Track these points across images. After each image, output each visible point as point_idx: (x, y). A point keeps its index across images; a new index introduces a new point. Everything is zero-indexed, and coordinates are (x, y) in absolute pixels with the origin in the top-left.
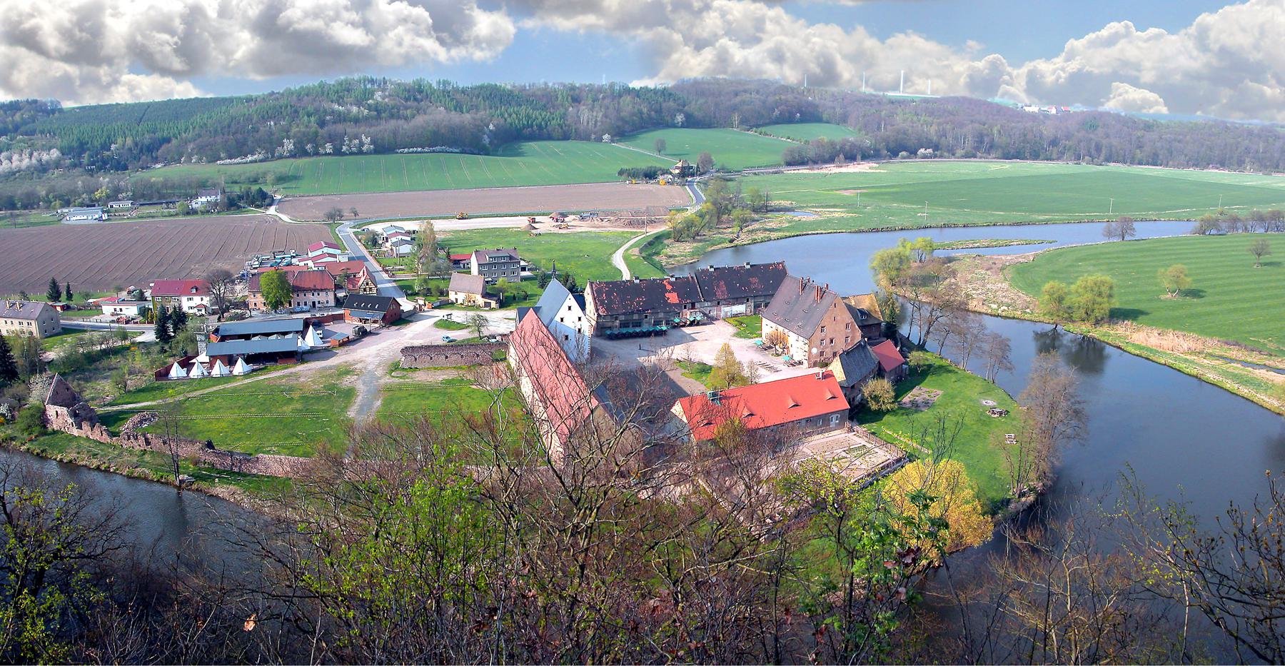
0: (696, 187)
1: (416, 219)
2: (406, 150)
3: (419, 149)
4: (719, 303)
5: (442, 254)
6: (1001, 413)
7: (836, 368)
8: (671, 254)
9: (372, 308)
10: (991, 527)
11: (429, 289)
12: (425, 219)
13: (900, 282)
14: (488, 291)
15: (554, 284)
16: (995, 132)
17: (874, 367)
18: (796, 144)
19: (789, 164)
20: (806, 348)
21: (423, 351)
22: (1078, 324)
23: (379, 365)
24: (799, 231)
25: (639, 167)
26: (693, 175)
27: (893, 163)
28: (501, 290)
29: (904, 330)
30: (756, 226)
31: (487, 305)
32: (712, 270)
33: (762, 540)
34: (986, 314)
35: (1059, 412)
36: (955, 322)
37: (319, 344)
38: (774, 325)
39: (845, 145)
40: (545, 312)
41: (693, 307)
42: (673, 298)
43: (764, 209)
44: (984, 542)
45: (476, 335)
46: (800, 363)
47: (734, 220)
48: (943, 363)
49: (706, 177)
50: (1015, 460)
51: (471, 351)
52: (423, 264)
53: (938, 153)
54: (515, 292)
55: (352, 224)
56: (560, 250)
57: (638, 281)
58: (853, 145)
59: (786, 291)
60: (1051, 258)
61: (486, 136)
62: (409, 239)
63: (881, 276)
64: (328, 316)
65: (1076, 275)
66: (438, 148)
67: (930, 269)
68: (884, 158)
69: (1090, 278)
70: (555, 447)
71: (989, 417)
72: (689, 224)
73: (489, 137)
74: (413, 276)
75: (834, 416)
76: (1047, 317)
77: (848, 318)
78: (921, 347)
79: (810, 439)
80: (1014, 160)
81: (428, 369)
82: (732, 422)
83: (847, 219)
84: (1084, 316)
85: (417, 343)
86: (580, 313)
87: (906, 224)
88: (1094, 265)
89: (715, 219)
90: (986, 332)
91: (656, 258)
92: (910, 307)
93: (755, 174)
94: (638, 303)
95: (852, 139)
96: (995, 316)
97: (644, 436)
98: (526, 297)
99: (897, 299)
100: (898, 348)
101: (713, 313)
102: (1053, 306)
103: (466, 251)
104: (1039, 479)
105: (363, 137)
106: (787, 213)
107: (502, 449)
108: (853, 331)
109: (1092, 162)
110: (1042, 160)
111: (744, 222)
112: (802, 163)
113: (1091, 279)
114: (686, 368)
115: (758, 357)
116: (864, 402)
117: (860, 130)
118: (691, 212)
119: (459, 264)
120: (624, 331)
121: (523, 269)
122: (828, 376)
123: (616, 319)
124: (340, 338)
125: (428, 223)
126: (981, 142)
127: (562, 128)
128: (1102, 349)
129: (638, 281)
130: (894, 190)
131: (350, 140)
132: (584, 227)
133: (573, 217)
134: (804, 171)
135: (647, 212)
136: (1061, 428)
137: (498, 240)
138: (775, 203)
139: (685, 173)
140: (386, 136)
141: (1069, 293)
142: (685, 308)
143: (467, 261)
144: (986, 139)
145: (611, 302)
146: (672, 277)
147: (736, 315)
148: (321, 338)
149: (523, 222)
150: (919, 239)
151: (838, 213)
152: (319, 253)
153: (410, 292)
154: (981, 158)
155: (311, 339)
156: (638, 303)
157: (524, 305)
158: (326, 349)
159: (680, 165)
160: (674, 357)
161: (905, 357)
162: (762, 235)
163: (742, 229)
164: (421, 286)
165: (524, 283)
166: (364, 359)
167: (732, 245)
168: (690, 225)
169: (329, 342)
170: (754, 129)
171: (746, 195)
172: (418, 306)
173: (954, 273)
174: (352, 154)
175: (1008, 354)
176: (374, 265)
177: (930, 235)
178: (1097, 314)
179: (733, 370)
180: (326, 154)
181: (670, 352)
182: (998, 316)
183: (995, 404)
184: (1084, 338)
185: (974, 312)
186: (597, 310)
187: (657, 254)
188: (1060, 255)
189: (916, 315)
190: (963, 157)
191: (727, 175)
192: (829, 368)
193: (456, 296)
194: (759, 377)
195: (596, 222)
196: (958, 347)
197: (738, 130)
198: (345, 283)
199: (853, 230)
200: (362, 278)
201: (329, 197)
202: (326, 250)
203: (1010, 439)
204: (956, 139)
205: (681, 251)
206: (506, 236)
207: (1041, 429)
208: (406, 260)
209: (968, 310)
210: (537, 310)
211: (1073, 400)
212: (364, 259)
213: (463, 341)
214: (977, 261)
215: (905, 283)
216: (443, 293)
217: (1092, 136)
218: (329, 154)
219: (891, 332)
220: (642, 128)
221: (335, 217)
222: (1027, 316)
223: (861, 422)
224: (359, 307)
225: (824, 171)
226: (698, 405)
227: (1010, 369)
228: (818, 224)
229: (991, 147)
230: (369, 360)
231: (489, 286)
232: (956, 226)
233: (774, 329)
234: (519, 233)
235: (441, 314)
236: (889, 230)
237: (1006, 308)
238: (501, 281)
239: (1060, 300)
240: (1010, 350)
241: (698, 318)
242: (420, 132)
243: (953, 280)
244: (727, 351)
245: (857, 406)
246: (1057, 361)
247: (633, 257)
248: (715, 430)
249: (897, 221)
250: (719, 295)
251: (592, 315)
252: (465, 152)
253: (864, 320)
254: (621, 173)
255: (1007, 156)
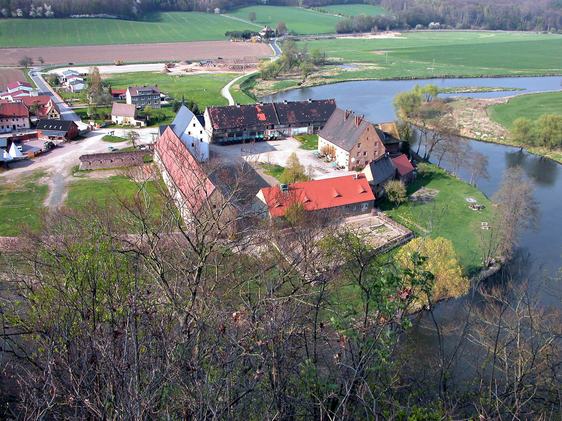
0: (275, 44)
1: (87, 66)
2: (77, 16)
3: (87, 16)
4: (290, 126)
5: (106, 90)
6: (479, 208)
7: (367, 172)
8: (260, 88)
9: (57, 129)
10: (468, 285)
11: (97, 115)
12: (93, 65)
13: (413, 115)
14: (138, 115)
15: (184, 109)
16: (485, 10)
17: (393, 172)
18: (345, 18)
19: (340, 32)
20: (348, 157)
21: (95, 158)
22: (537, 148)
23: (64, 169)
24: (344, 79)
25: (238, 30)
26: (274, 36)
27: (412, 32)
28: (147, 114)
29: (414, 148)
30: (316, 74)
31: (138, 124)
32: (286, 103)
33: (312, 284)
34: (473, 139)
35: (520, 209)
36: (450, 144)
37: (20, 155)
38: (327, 142)
39: (379, 19)
40: (178, 128)
41: (273, 128)
42: (262, 117)
43: (322, 63)
44: (462, 295)
45: (132, 145)
46: (343, 168)
47: (301, 70)
48: (441, 171)
49: (282, 38)
50: (487, 241)
51: (129, 157)
52: (92, 97)
53: (443, 25)
54: (157, 116)
55: (40, 68)
56: (187, 86)
57: (239, 106)
58: (384, 19)
59: (335, 119)
60: (521, 101)
61: (134, 8)
62: (82, 79)
63: (400, 111)
64: (25, 135)
65: (538, 113)
66: (101, 15)
67: (435, 106)
68: (406, 28)
69: (549, 115)
70: (185, 214)
71: (471, 210)
72: (272, 69)
73: (137, 8)
74: (86, 106)
75: (365, 204)
76: (516, 142)
77: (376, 138)
78: (426, 160)
79: (347, 219)
80: (498, 31)
81: (100, 170)
82: (297, 206)
83: (378, 71)
84: (543, 142)
85: (91, 152)
86: (201, 128)
87: (419, 75)
88: (552, 107)
89: (288, 66)
90: (471, 151)
91: (251, 91)
92: (419, 132)
93: (316, 39)
94: (240, 121)
95: (383, 15)
96: (478, 140)
97: (238, 211)
98: (165, 119)
99: (410, 126)
100: (410, 161)
101: (286, 132)
102: (520, 135)
103: (122, 88)
104: (503, 254)
105: (46, 6)
106: (338, 66)
107: (148, 221)
108: (380, 146)
109: (556, 31)
110: (519, 30)
111: (308, 72)
112: (348, 31)
113: (550, 116)
114: (266, 168)
115: (315, 163)
116: (385, 196)
117: (389, 9)
118: (273, 60)
119: (118, 97)
120: (231, 139)
121: (163, 99)
122: (361, 177)
123: (226, 131)
124: (36, 151)
125: (95, 68)
126: (475, 17)
127: (187, 3)
128: (555, 166)
129: (239, 106)
130: (410, 51)
131: (36, 7)
132: (203, 71)
133: (196, 64)
134: (350, 37)
135: (245, 60)
136: (521, 220)
137: (145, 80)
138: (329, 59)
139: (269, 35)
140: (62, 4)
141: (533, 126)
142: (267, 128)
143: (123, 95)
144: (478, 16)
145: (222, 120)
146: (261, 103)
147: (301, 134)
148: (21, 151)
149: (161, 67)
150: (427, 85)
151: (372, 67)
152: (16, 90)
153: (84, 117)
154: (474, 29)
155: (14, 152)
156: (240, 121)
157: (164, 124)
158: (26, 159)
159: (265, 29)
160: (259, 160)
161: (415, 166)
162: (321, 81)
163: (306, 76)
164: (91, 112)
165: (163, 109)
166: (53, 165)
167: (300, 87)
168: (272, 69)
169: (27, 154)
170: (312, 8)
171: (310, 53)
172: (90, 127)
173: (451, 110)
174: (37, 17)
175: (486, 167)
176: (58, 99)
177: (436, 83)
178: (553, 141)
179: (298, 171)
180: (18, 17)
181: (257, 157)
182: (481, 140)
183: (475, 201)
184: (541, 158)
185: (464, 137)
186: (213, 126)
187: (252, 88)
188: (528, 99)
189: (424, 138)
190: (461, 28)
191: (295, 37)
192: (362, 172)
193: (117, 119)
194: (315, 176)
195: (211, 67)
196: (452, 161)
197: (302, 8)
198: (37, 112)
199: (382, 79)
200: (49, 107)
201: (20, 49)
202: (22, 88)
203: (484, 226)
204: (456, 15)
205: (268, 85)
206: (150, 77)
207: (507, 220)
208: (81, 94)
209: (459, 136)
210: (172, 127)
211: (531, 201)
212: (50, 94)
213: (123, 150)
214: (468, 102)
215: (416, 116)
216: (108, 117)
217: (557, 12)
218: (20, 17)
219: (406, 148)
220: (241, 4)
221: (26, 63)
222: (501, 141)
223: (382, 210)
224: (47, 128)
225: (364, 38)
226: (274, 193)
227: (487, 178)
228: (358, 74)
229: (482, 21)
230: (57, 165)
231: (139, 112)
232: (454, 77)
233: (326, 144)
234: (158, 75)
235: (107, 131)
236: (407, 79)
237: (486, 135)
238: (147, 108)
239: (526, 131)
240: (488, 165)
241: (276, 136)
242: (87, 3)
243: (450, 115)
244: (294, 158)
245: (380, 199)
246: (520, 172)
247: (236, 91)
248: (285, 210)
249: (412, 73)
250: (291, 120)
251: (209, 129)
252: (120, 19)
253: (386, 138)
254: (227, 34)
255: (493, 28)
